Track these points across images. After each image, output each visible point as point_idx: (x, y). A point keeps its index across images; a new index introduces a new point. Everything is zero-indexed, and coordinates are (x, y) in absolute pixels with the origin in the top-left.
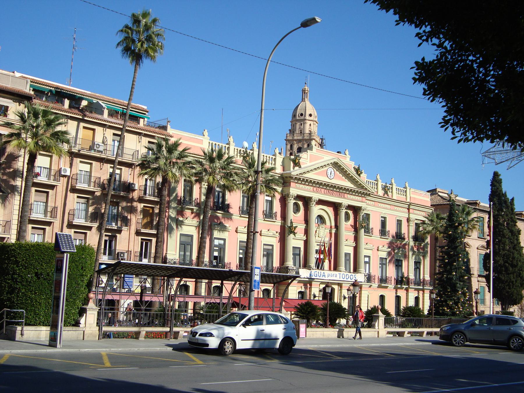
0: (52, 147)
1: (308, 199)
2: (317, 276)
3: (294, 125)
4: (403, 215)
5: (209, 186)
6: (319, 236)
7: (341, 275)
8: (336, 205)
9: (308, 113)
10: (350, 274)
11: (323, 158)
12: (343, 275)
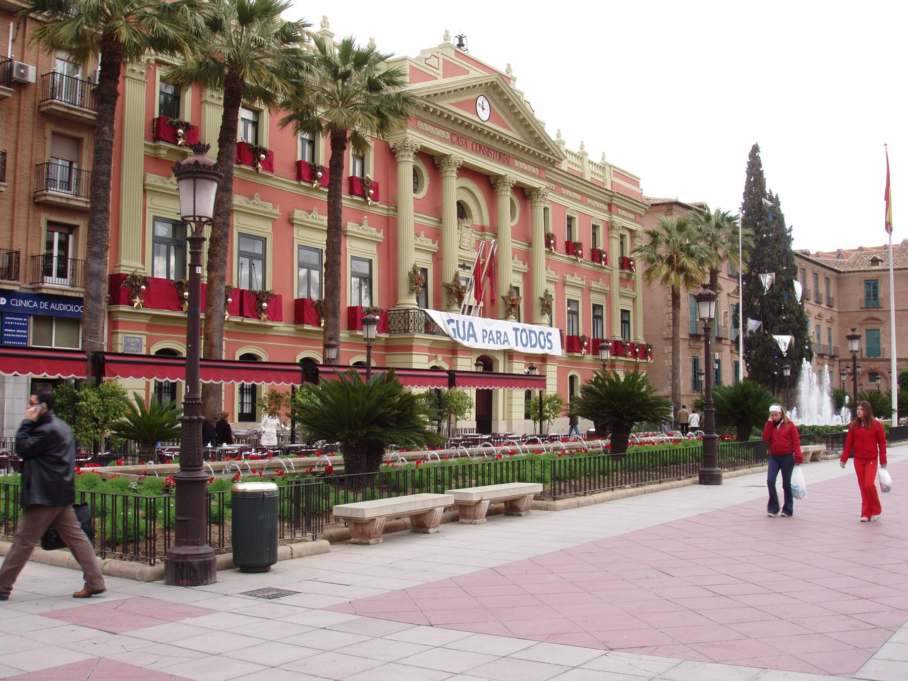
4: (600, 216)
6: (462, 247)
11: (468, 72)
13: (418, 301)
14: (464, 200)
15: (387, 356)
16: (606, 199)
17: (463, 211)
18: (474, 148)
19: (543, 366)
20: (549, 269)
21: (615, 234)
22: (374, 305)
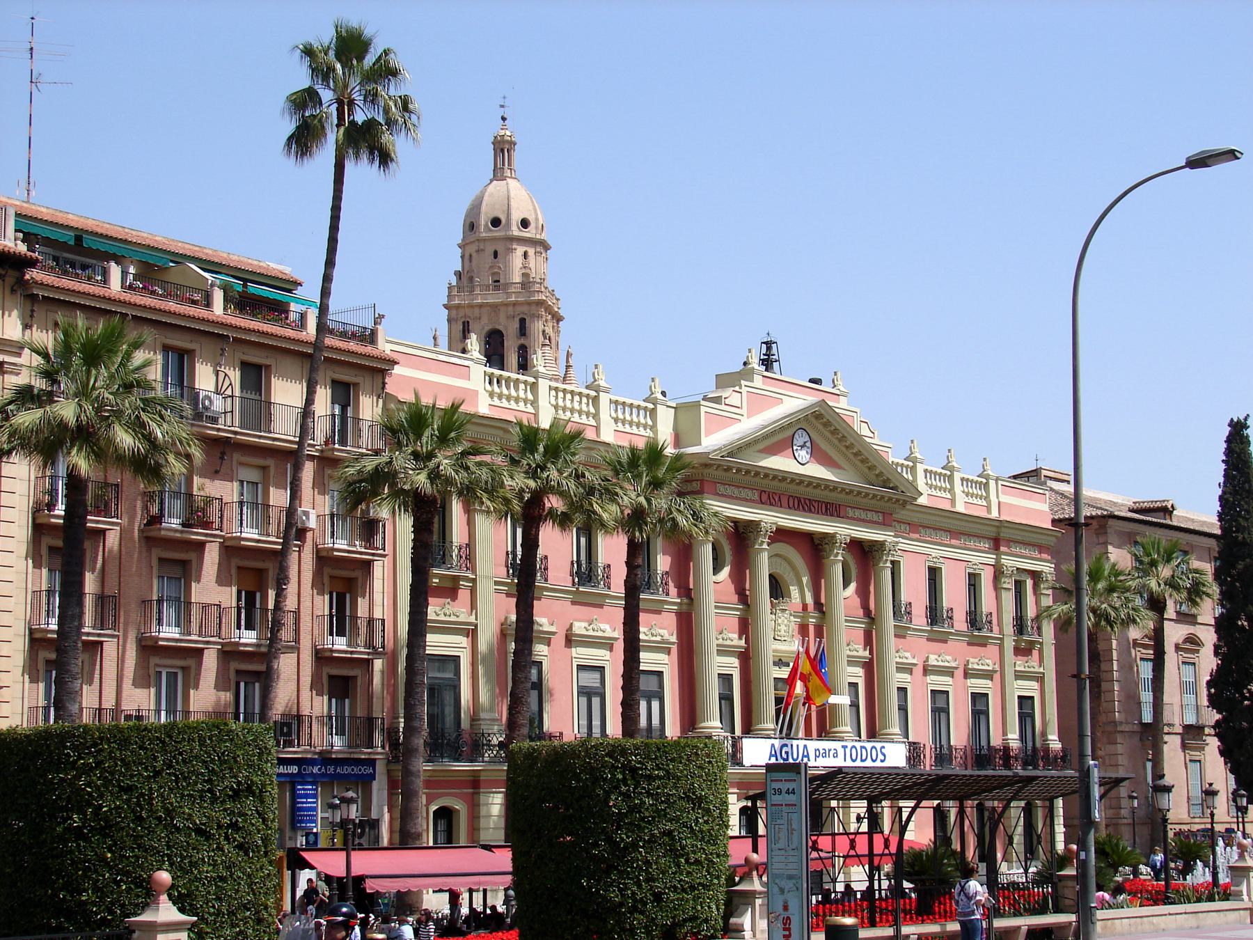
3: (471, 256)
6: (777, 638)
7: (848, 750)
8: (817, 542)
9: (516, 217)
12: (854, 750)
13: (721, 723)
14: (778, 571)
16: (991, 532)
17: (777, 589)
18: (791, 505)
20: (1169, 506)
21: (1008, 583)
22: (608, 732)
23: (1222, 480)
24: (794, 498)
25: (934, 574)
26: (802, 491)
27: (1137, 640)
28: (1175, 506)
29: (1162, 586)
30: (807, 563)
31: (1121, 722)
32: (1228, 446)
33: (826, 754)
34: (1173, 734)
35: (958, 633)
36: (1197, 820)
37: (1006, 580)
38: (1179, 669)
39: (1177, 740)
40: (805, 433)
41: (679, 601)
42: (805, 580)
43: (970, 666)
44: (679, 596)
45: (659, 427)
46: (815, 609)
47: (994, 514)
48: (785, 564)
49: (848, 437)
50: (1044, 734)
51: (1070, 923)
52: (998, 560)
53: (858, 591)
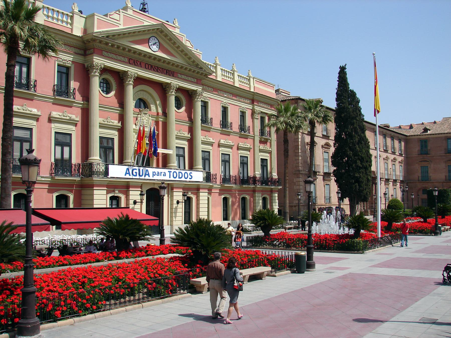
0: (48, 41)
1: (165, 86)
2: (136, 176)
5: (287, 114)
7: (172, 174)
8: (164, 87)
10: (183, 172)
15: (82, 191)
16: (251, 97)
19: (198, 193)
20: (321, 100)
21: (259, 117)
22: (231, 174)
23: (337, 87)
24: (149, 65)
25: (225, 110)
26: (151, 61)
27: (308, 142)
28: (323, 100)
29: (313, 116)
30: (158, 95)
31: (302, 170)
32: (339, 75)
33: (158, 174)
34: (320, 175)
35: (234, 132)
36: (327, 204)
37: (256, 115)
38: (323, 154)
39: (321, 177)
40: (156, 39)
41: (83, 102)
42: (158, 102)
43: (240, 145)
44: (83, 100)
45: (75, 24)
46: (162, 115)
47: (252, 90)
48: (145, 93)
49: (177, 43)
50: (271, 173)
51: (292, 227)
52: (253, 107)
53: (186, 111)
